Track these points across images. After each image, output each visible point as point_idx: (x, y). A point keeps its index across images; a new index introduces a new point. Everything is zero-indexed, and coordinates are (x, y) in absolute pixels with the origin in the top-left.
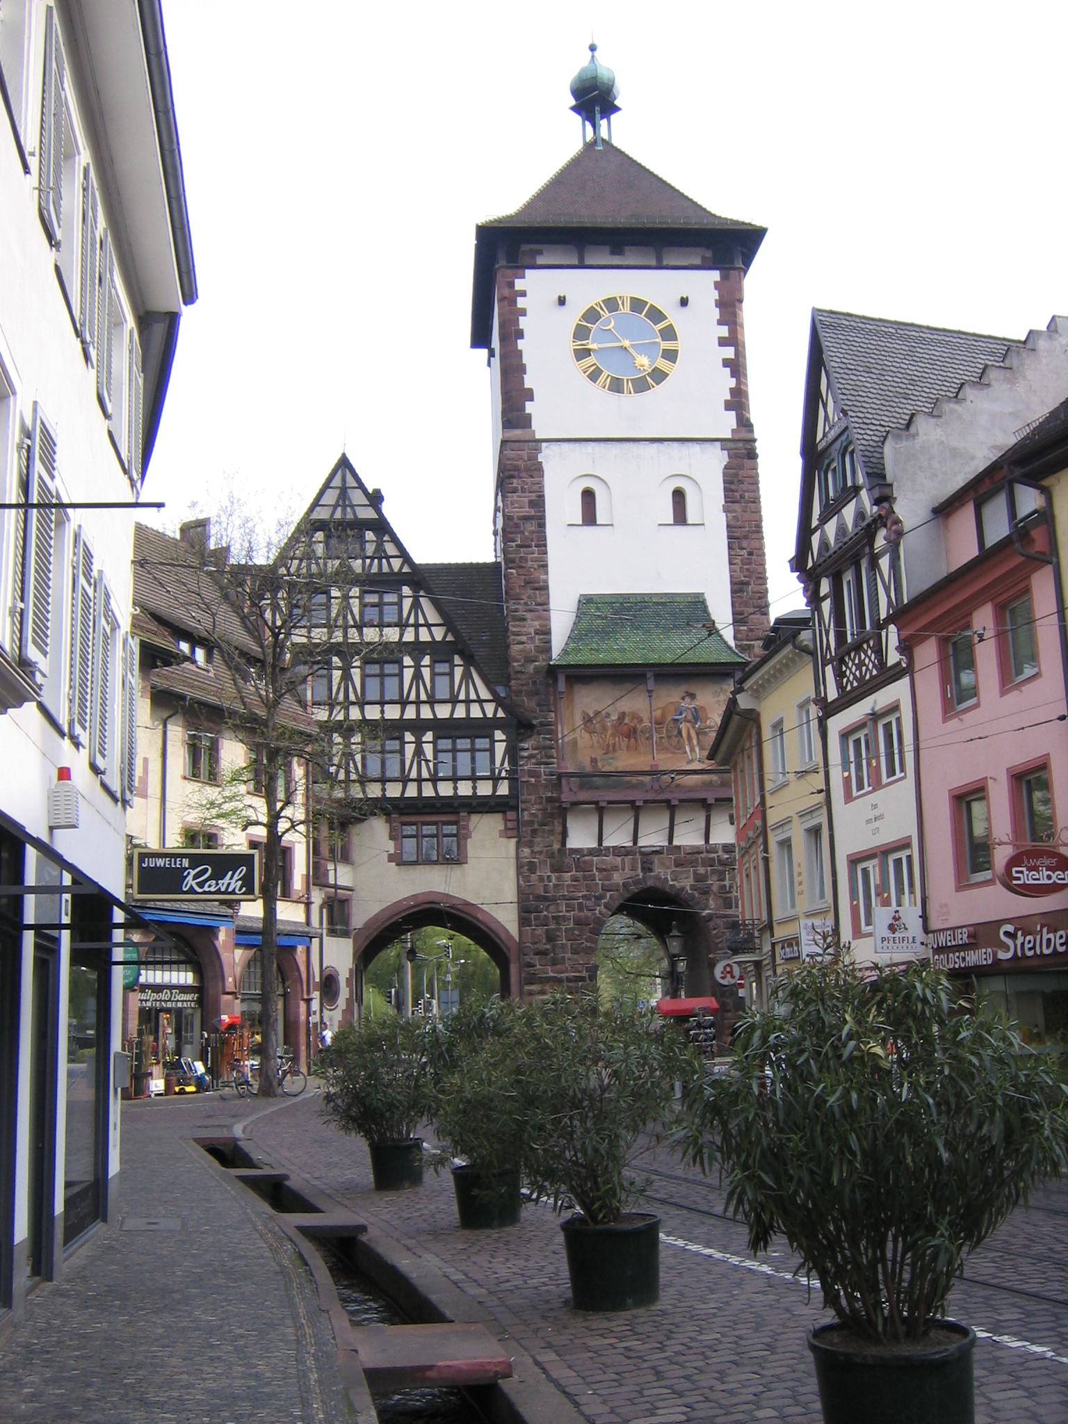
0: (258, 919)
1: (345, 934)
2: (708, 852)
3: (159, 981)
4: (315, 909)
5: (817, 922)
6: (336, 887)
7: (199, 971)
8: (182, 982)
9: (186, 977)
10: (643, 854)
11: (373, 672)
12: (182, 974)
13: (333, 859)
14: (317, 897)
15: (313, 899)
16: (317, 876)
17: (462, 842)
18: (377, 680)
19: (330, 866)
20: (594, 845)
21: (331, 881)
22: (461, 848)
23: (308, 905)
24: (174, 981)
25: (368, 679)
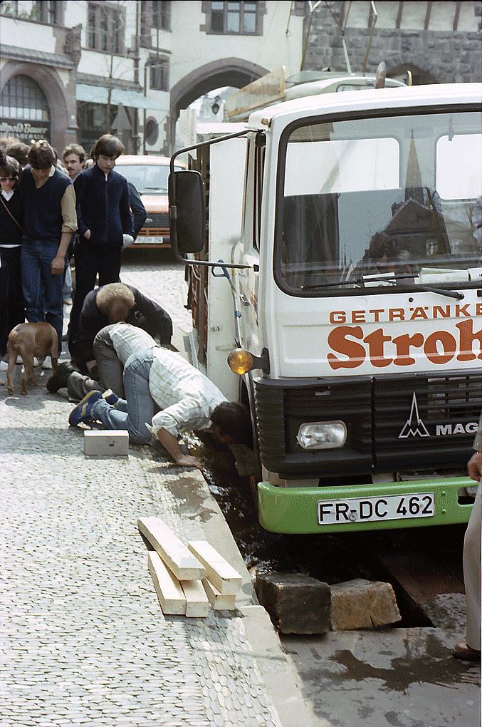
0: (292, 4)
1: (163, 87)
2: (456, 37)
3: (13, 116)
4: (142, 63)
5: (360, 57)
6: (157, 49)
7: (47, 109)
8: (33, 118)
9: (37, 114)
10: (403, 36)
11: (234, 9)
12: (33, 111)
13: (156, 25)
14: (144, 55)
15: (140, 57)
16: (143, 40)
17: (259, 17)
18: (237, 15)
19: (154, 31)
20: (420, 28)
21: (154, 45)
22: (259, 23)
23: (136, 61)
24: (26, 117)
25: (363, 505)
